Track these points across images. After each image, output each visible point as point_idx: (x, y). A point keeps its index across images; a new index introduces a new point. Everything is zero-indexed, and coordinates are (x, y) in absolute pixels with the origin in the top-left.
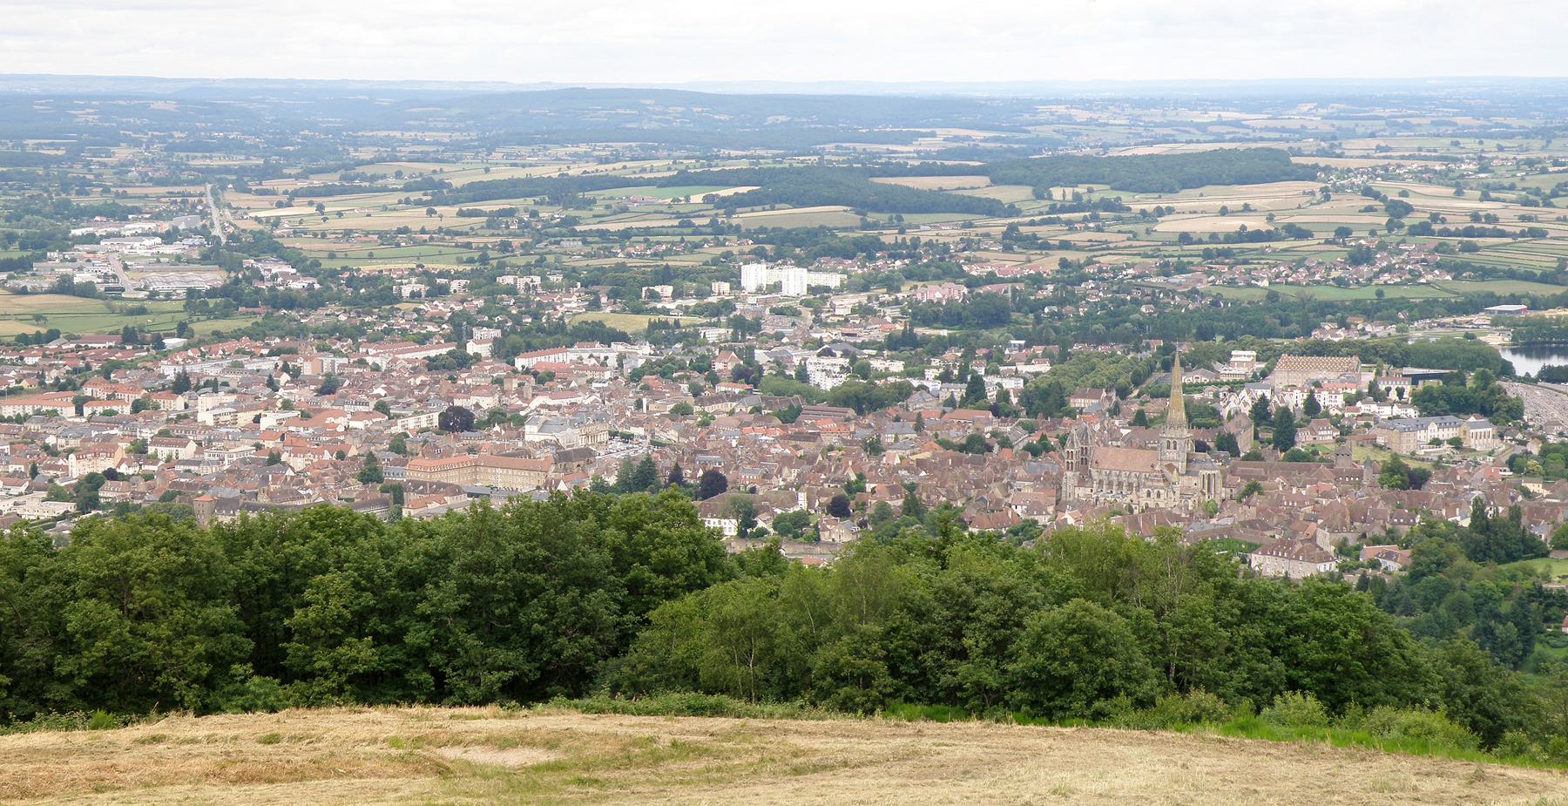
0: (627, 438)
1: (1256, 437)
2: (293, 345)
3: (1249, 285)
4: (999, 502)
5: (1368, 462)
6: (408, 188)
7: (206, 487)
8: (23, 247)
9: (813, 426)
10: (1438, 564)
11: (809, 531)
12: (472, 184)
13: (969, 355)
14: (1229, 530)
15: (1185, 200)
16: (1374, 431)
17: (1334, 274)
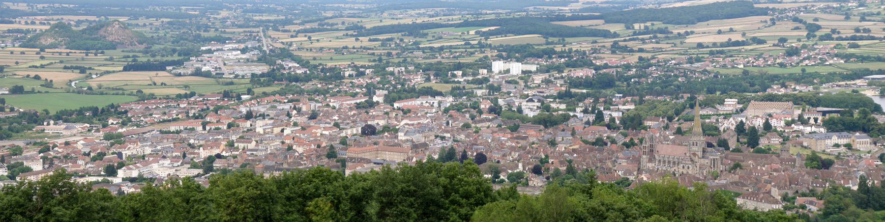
0: (443, 138)
1: (738, 141)
2: (299, 98)
3: (733, 67)
4: (610, 169)
5: (799, 155)
6: (347, 29)
7: (260, 161)
8: (180, 55)
9: (525, 133)
10: (840, 209)
11: (523, 181)
12: (375, 27)
13: (596, 101)
14: (725, 186)
15: (700, 28)
16: (801, 139)
17: (778, 61)
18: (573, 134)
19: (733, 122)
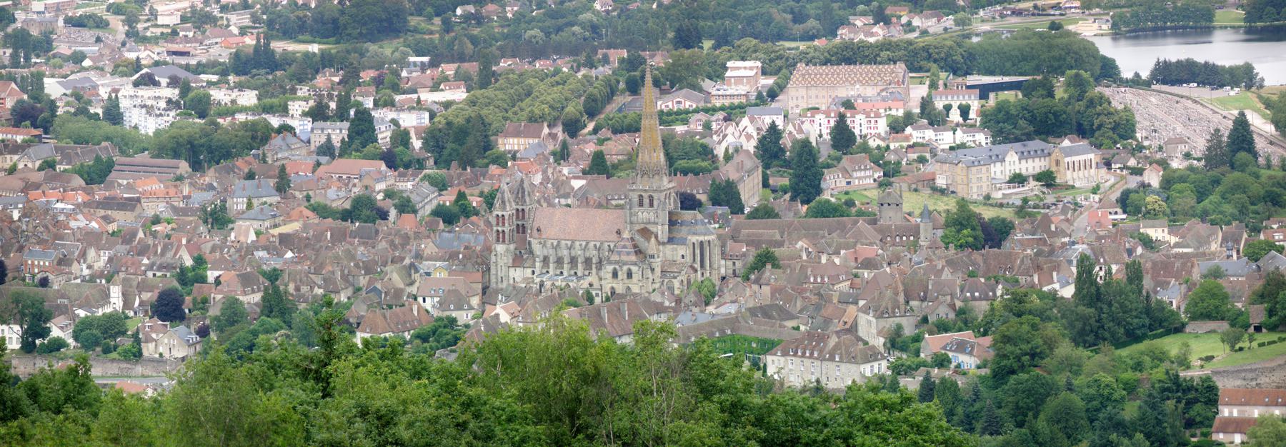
1: (765, 184)
4: (398, 293)
5: (926, 214)
9: (130, 188)
11: (125, 342)
13: (351, 80)
14: (732, 321)
18: (283, 186)
19: (751, 130)
